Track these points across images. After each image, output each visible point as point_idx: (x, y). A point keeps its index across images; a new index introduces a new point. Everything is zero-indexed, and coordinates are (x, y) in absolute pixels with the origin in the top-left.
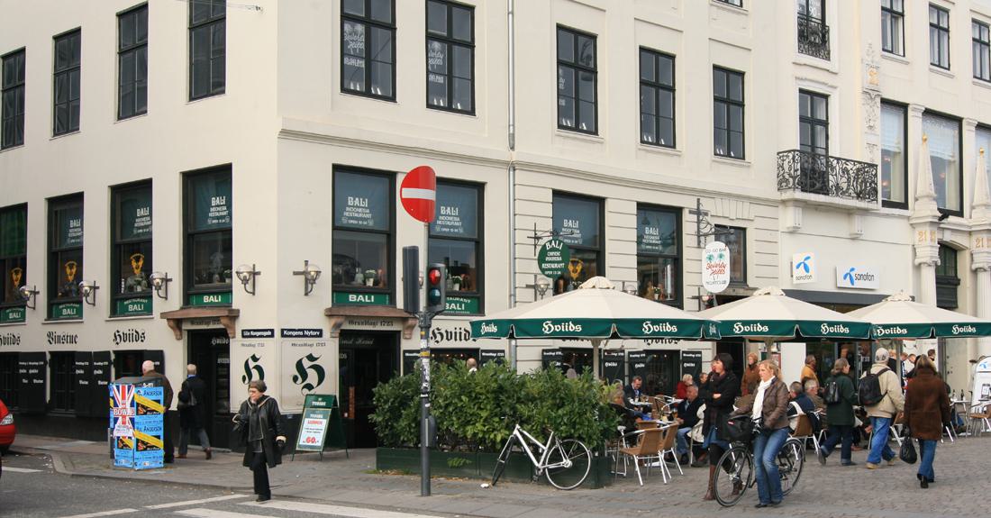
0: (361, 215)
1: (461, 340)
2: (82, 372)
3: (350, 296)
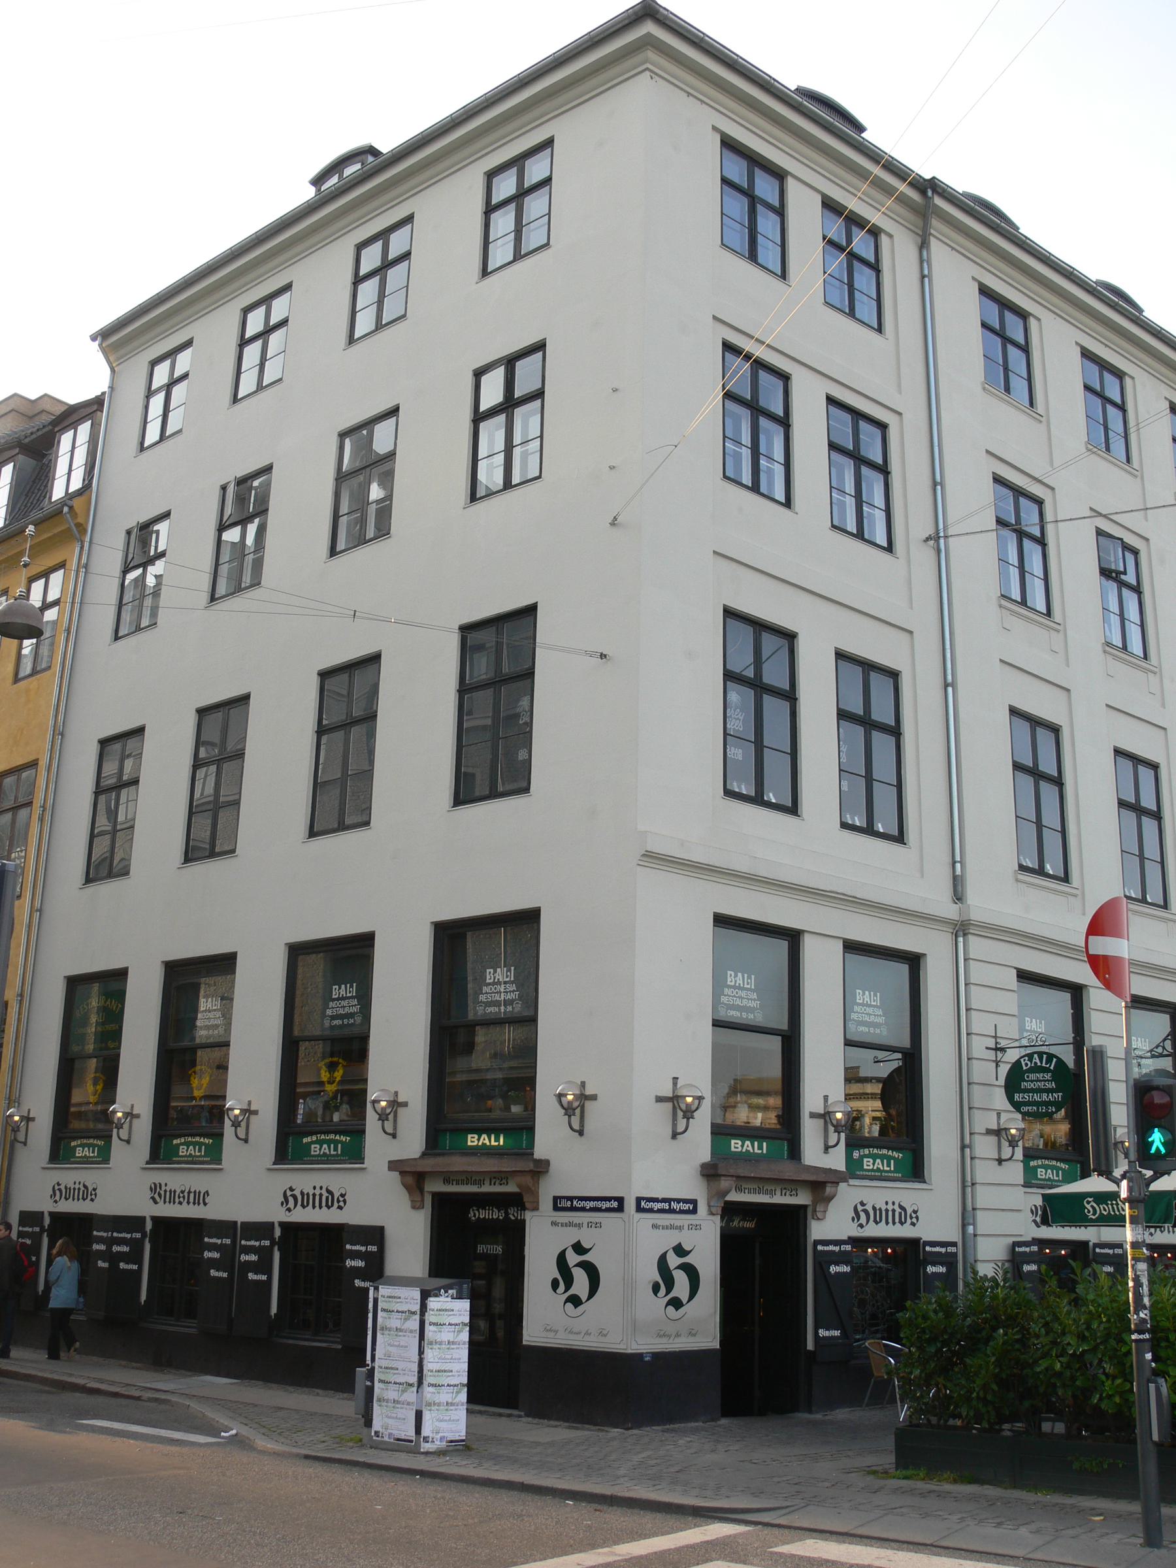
0: (745, 1002)
1: (894, 1223)
2: (216, 1255)
3: (733, 1142)
